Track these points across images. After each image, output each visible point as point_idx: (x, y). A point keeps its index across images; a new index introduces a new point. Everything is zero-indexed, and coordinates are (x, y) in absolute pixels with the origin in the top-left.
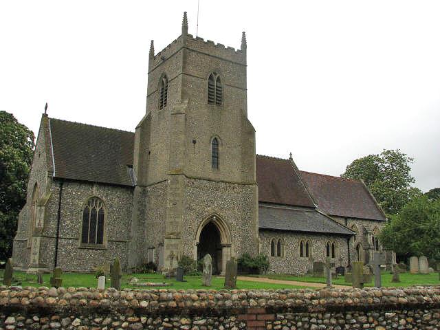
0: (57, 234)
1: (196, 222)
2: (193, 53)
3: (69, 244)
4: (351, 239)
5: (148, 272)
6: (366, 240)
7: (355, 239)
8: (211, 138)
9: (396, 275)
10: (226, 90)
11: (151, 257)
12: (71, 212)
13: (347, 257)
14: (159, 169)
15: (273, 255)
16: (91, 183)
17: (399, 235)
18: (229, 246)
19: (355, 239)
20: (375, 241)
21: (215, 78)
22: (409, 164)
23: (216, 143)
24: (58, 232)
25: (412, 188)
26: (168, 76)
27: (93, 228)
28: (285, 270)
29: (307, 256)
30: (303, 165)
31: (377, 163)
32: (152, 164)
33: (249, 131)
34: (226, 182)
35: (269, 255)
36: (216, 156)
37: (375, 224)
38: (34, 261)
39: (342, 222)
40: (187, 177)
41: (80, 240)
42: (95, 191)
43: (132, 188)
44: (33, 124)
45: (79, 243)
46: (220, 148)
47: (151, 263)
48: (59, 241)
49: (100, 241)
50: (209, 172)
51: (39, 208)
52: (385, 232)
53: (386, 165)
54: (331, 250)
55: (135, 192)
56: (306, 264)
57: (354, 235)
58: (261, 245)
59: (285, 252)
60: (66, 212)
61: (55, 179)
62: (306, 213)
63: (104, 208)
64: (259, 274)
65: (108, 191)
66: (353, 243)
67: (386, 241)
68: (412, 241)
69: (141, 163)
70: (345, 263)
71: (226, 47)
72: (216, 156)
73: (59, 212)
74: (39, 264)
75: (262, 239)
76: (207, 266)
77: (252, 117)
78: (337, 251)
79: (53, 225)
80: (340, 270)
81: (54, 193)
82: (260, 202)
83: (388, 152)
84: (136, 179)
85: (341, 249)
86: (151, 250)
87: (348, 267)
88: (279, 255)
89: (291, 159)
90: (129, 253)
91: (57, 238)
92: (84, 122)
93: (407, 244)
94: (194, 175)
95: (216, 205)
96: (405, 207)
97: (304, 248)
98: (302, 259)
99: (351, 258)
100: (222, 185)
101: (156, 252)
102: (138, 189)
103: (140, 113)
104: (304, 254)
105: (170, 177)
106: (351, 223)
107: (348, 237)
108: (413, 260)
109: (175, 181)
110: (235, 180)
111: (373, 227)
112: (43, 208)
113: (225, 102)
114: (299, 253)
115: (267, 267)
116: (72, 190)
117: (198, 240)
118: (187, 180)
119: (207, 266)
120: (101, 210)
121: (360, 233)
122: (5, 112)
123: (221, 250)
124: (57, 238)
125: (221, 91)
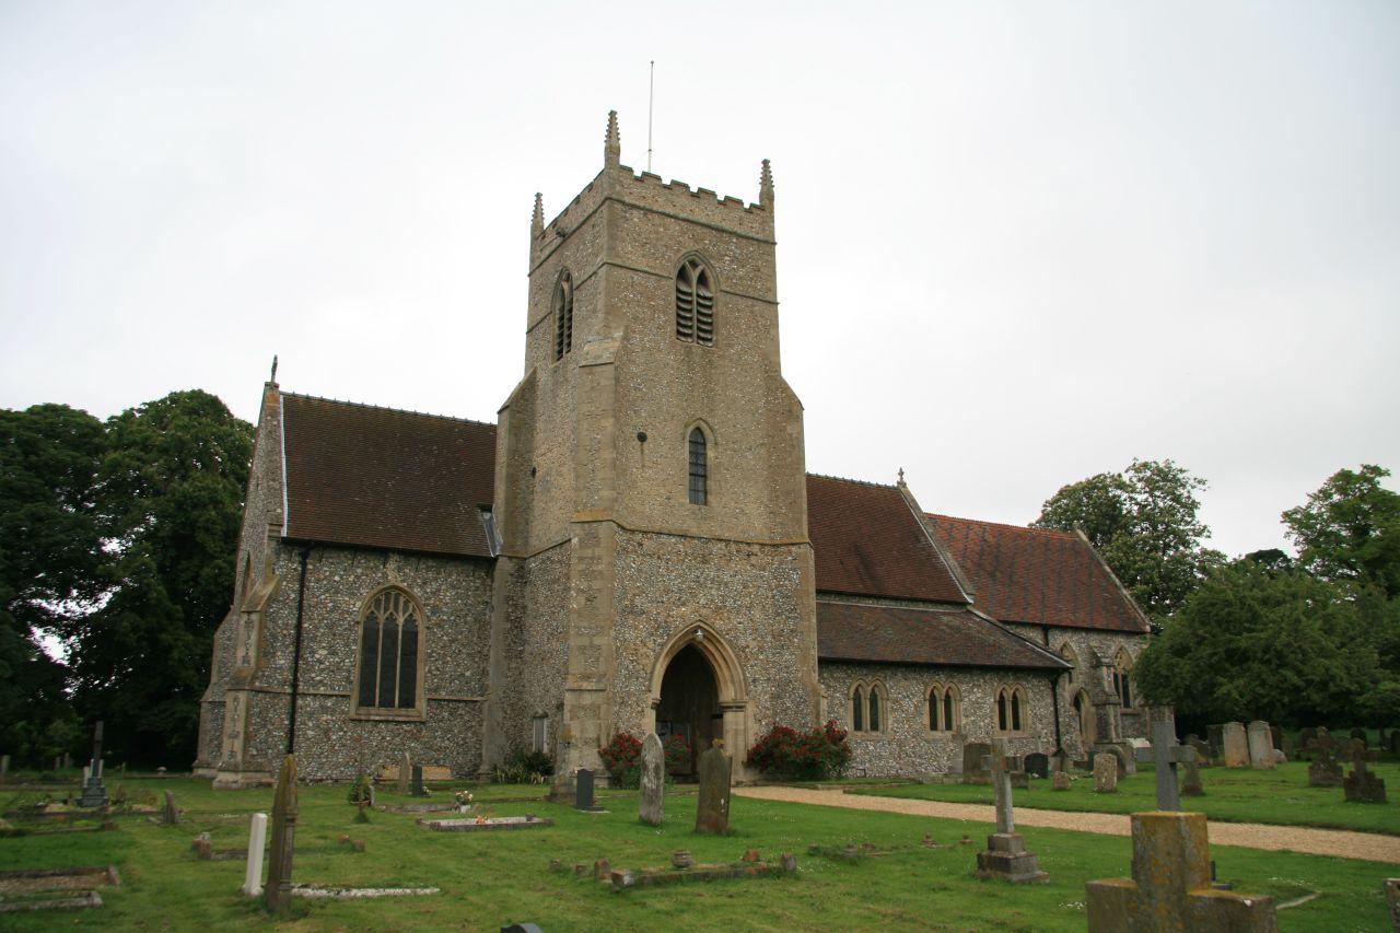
0: (295, 685)
1: (651, 645)
2: (635, 212)
3: (325, 709)
4: (1061, 680)
5: (527, 781)
6: (1098, 682)
7: (1071, 681)
8: (686, 426)
9: (1192, 776)
10: (722, 308)
11: (540, 739)
12: (331, 626)
13: (1053, 728)
14: (551, 518)
15: (858, 726)
16: (383, 552)
17: (1185, 666)
18: (740, 708)
19: (1071, 681)
20: (1121, 682)
21: (694, 275)
22: (1196, 495)
23: (698, 442)
24: (296, 679)
25: (1204, 552)
26: (575, 275)
27: (389, 665)
28: (892, 766)
29: (949, 726)
30: (931, 499)
31: (1119, 492)
32: (539, 503)
33: (788, 409)
34: (728, 541)
35: (849, 726)
36: (699, 473)
37: (1121, 640)
38: (233, 754)
39: (1036, 636)
40: (623, 528)
41: (354, 701)
42: (393, 573)
43: (490, 563)
44: (245, 407)
45: (351, 707)
46: (711, 454)
47: (539, 754)
48: (300, 702)
49: (408, 702)
50: (683, 514)
51: (245, 617)
52: (1146, 661)
53: (1140, 498)
54: (1010, 712)
55: (497, 573)
56: (944, 753)
57: (1067, 670)
58: (824, 704)
59: (890, 721)
60: (316, 628)
61: (287, 544)
62: (945, 619)
63: (417, 616)
64: (818, 780)
65: (426, 570)
66: (1067, 690)
67: (1152, 680)
68: (1221, 679)
69: (511, 499)
70: (1045, 745)
71: (721, 197)
72: (699, 473)
73: (299, 627)
74: (244, 762)
75: (828, 687)
76: (651, 766)
77: (793, 371)
78: (1026, 713)
79: (283, 660)
80: (1036, 764)
81: (283, 577)
82: (819, 592)
83: (1145, 466)
84: (500, 538)
85: (1036, 704)
86: (539, 721)
87: (1055, 755)
88: (875, 726)
89: (902, 484)
90: (484, 730)
91: (294, 695)
92: (370, 402)
93: (1211, 687)
94: (644, 525)
95: (702, 601)
96: (1190, 600)
97: (941, 707)
98: (937, 734)
99: (1062, 729)
100: (718, 548)
101: (551, 726)
102: (504, 566)
103: (512, 375)
104: (941, 722)
105: (578, 529)
106: (1057, 640)
107: (1053, 674)
108: (1232, 733)
109: (591, 539)
110: (752, 535)
111: (1113, 649)
112: (254, 617)
113: (722, 333)
114: (926, 720)
115: (842, 757)
116: (329, 573)
117: (656, 694)
118: (621, 537)
119: (651, 766)
120: (410, 621)
121: (1082, 665)
122: (200, 392)
123: (721, 716)
124: (294, 695)
125: (710, 307)
